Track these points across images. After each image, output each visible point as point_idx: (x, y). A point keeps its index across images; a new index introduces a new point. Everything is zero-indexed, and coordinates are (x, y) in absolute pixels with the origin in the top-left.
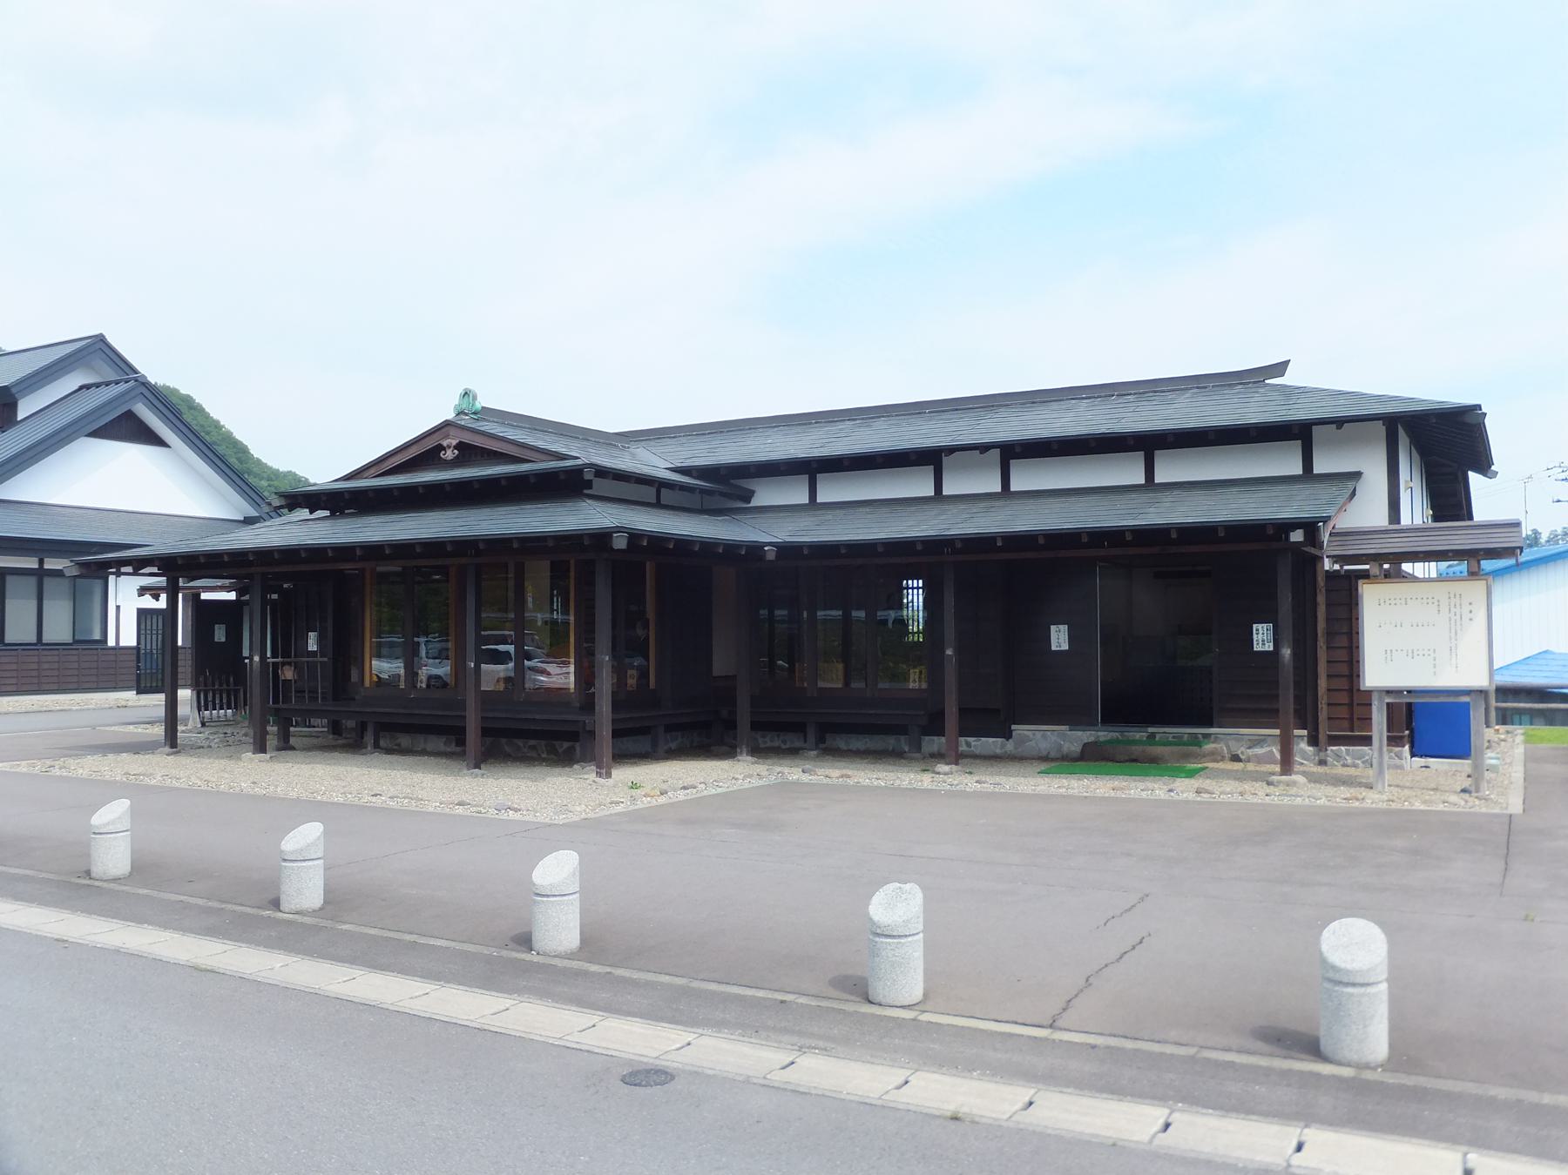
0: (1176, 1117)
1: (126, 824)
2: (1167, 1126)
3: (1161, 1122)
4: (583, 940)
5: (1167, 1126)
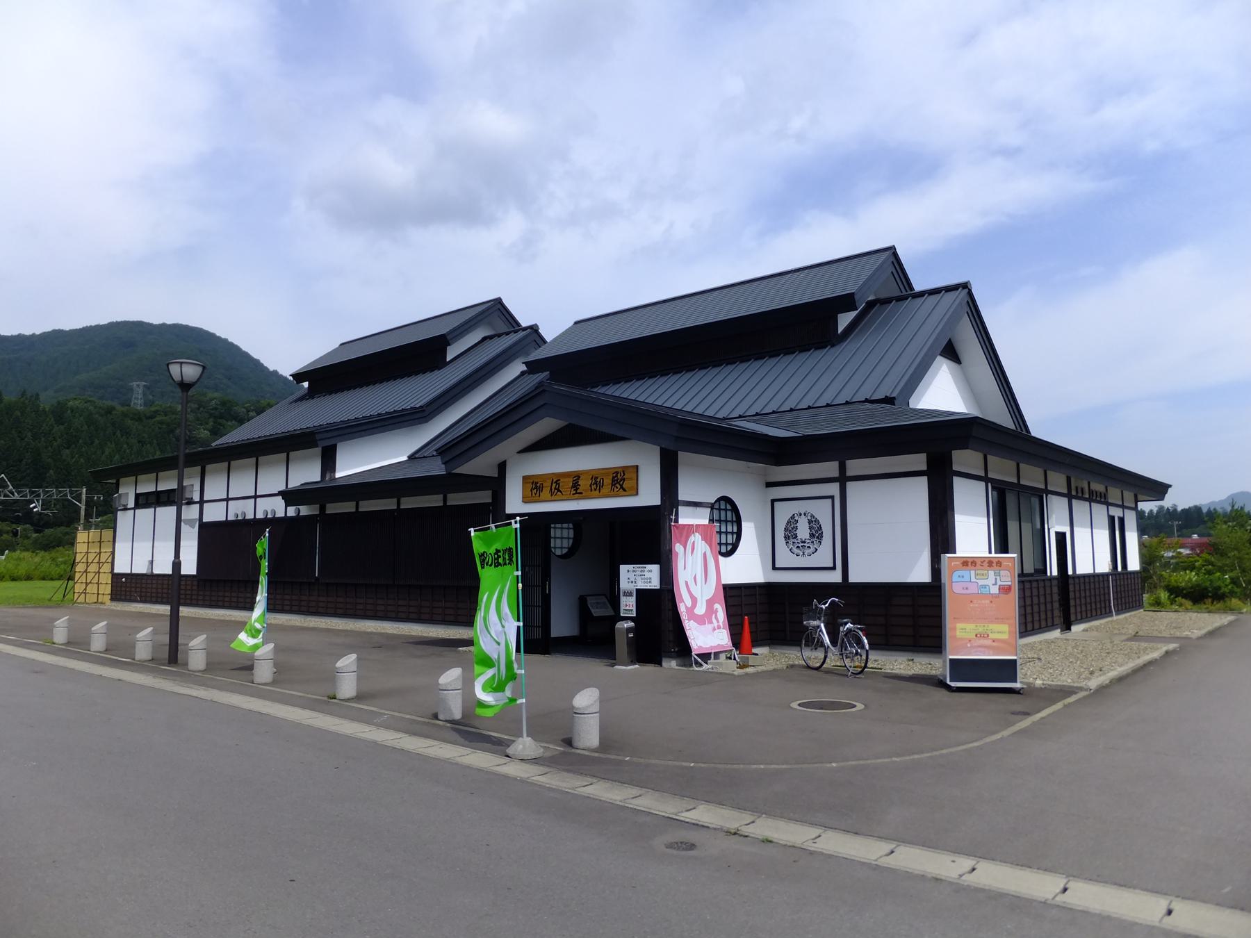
0: (1071, 885)
1: (596, 708)
2: (1065, 890)
3: (1062, 886)
4: (207, 664)
5: (1065, 890)
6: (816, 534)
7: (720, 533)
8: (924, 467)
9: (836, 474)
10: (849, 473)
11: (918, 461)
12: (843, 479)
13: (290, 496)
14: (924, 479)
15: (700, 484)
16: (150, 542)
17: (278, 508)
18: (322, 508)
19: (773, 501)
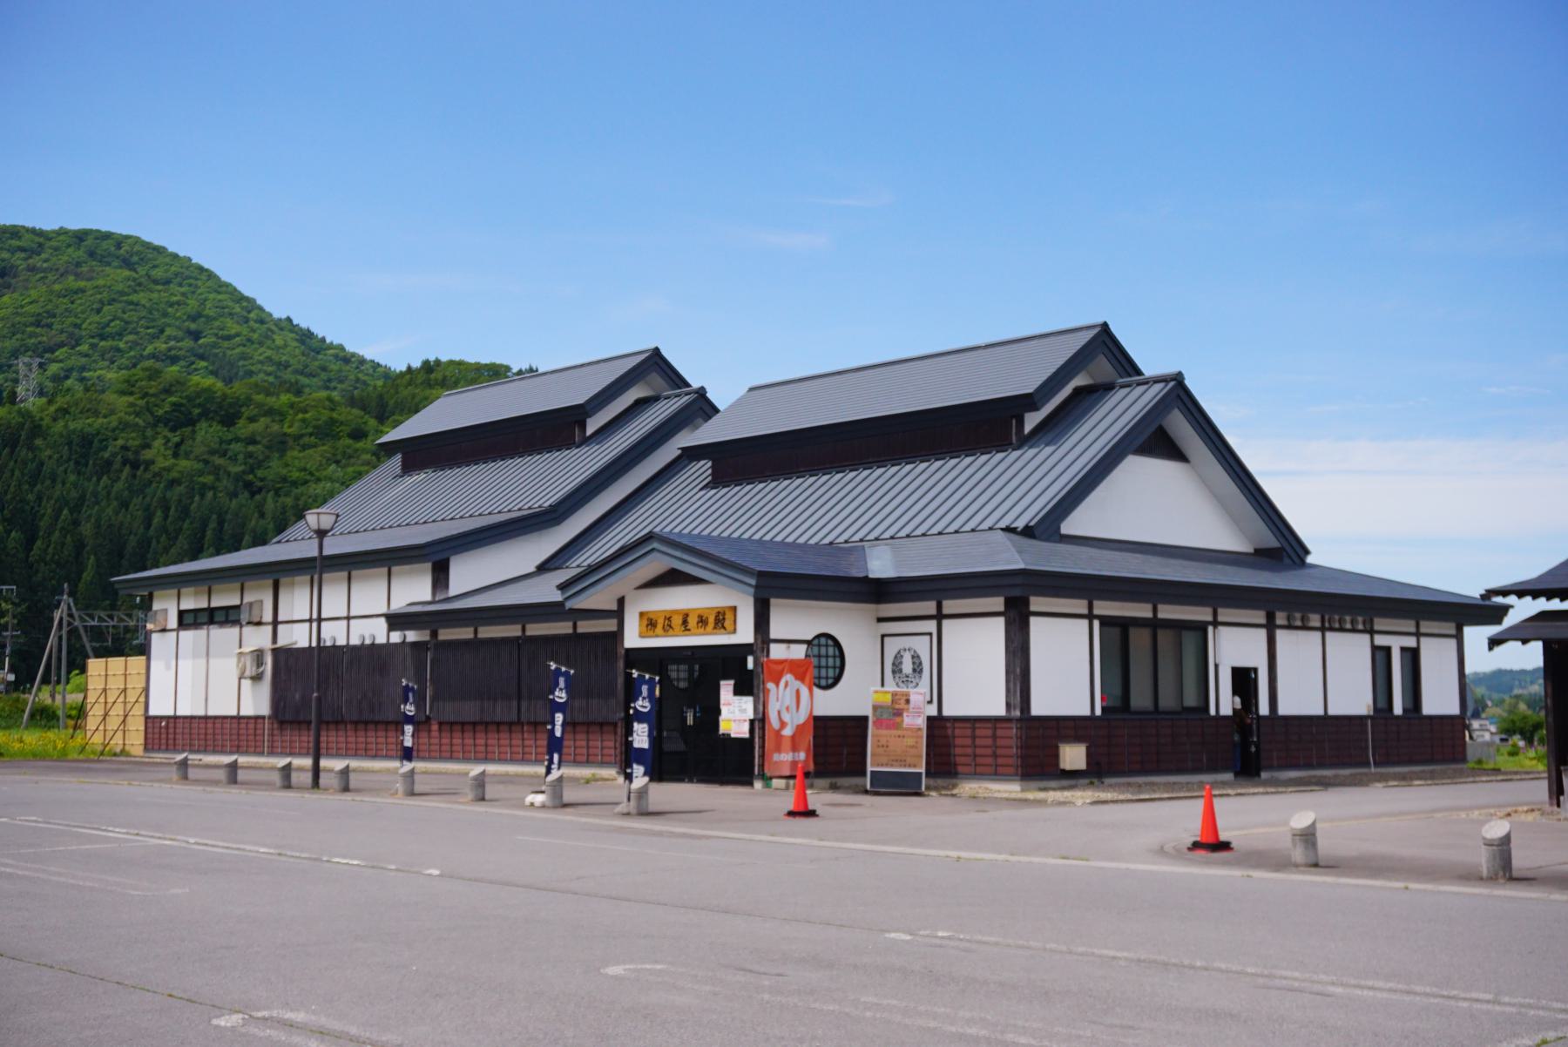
6: (918, 669)
7: (819, 667)
8: (1001, 608)
9: (933, 612)
10: (946, 611)
11: (998, 603)
12: (940, 617)
13: (396, 621)
14: (1001, 621)
15: (795, 623)
16: (196, 671)
17: (377, 632)
18: (434, 634)
19: (883, 636)
